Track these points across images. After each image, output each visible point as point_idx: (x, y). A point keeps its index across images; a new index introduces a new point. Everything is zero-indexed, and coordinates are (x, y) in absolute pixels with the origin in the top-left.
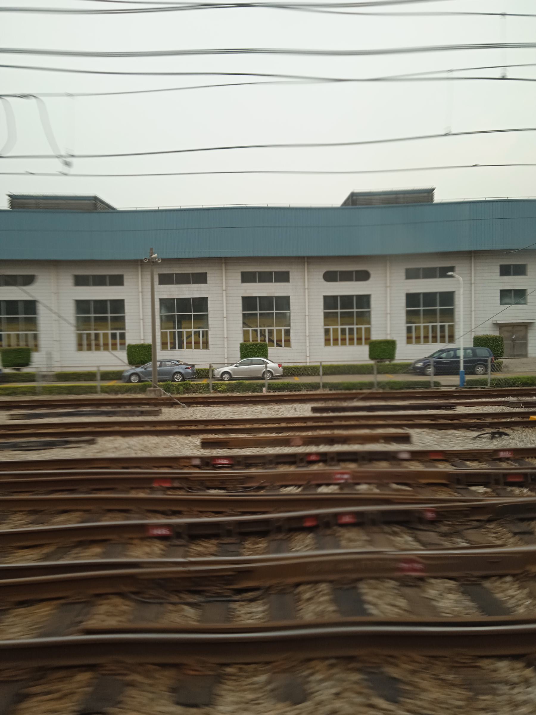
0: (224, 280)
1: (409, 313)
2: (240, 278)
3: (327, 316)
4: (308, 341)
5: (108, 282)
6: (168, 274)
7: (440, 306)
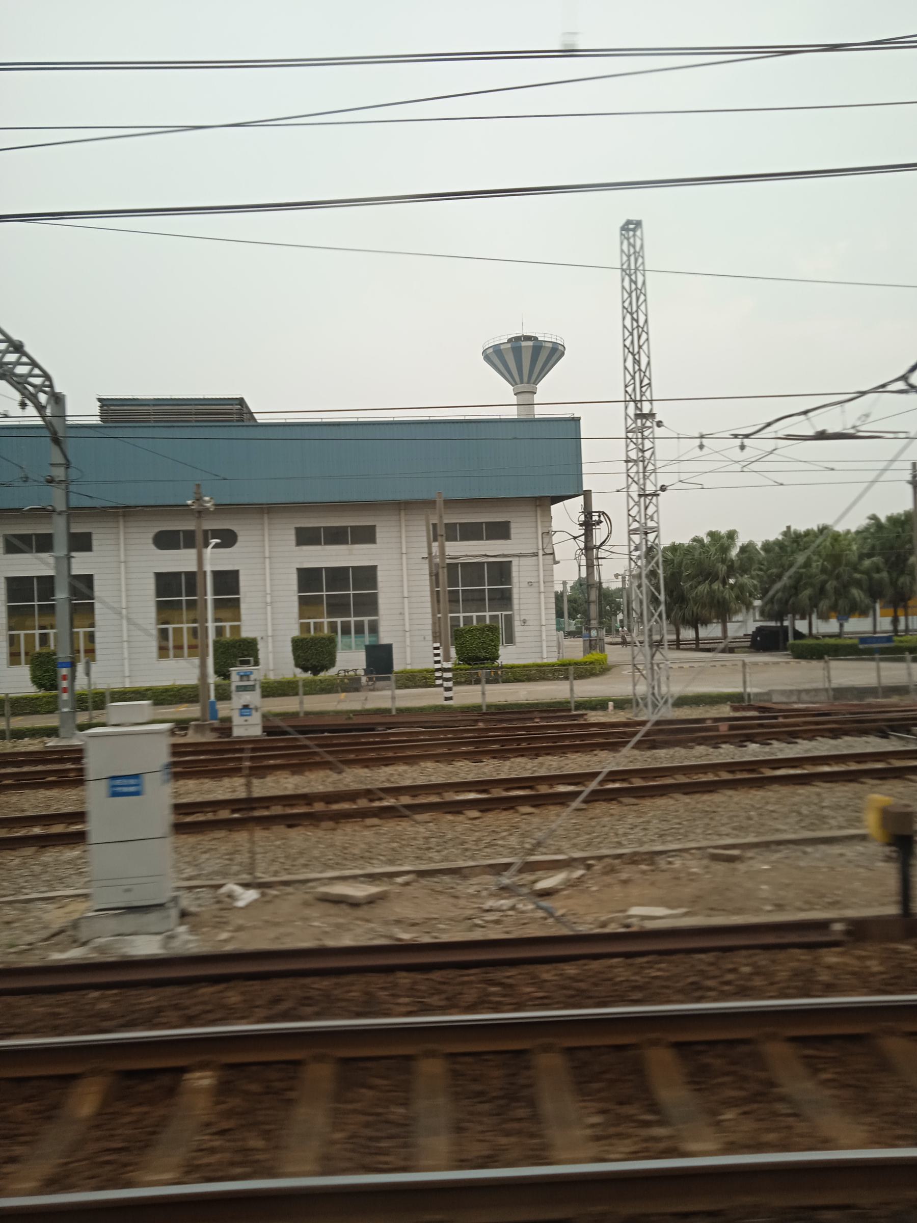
0: (122, 545)
1: (161, 607)
2: (292, 537)
3: (304, 602)
4: (126, 652)
5: (182, 544)
6: (499, 523)
7: (187, 596)
